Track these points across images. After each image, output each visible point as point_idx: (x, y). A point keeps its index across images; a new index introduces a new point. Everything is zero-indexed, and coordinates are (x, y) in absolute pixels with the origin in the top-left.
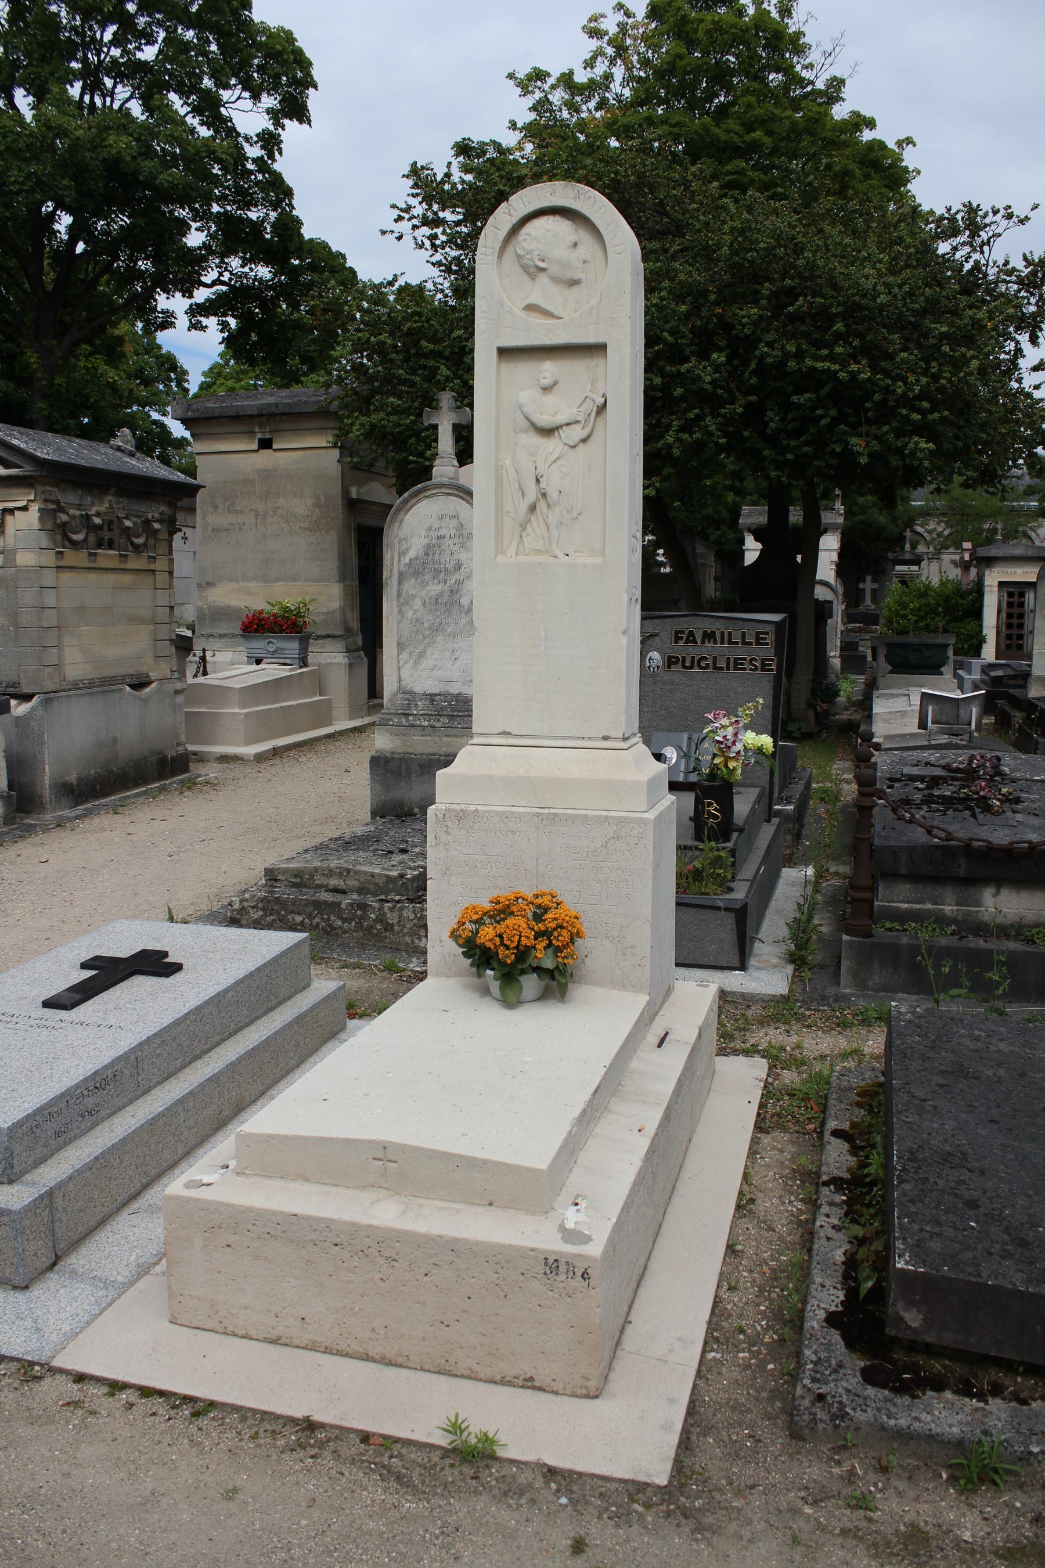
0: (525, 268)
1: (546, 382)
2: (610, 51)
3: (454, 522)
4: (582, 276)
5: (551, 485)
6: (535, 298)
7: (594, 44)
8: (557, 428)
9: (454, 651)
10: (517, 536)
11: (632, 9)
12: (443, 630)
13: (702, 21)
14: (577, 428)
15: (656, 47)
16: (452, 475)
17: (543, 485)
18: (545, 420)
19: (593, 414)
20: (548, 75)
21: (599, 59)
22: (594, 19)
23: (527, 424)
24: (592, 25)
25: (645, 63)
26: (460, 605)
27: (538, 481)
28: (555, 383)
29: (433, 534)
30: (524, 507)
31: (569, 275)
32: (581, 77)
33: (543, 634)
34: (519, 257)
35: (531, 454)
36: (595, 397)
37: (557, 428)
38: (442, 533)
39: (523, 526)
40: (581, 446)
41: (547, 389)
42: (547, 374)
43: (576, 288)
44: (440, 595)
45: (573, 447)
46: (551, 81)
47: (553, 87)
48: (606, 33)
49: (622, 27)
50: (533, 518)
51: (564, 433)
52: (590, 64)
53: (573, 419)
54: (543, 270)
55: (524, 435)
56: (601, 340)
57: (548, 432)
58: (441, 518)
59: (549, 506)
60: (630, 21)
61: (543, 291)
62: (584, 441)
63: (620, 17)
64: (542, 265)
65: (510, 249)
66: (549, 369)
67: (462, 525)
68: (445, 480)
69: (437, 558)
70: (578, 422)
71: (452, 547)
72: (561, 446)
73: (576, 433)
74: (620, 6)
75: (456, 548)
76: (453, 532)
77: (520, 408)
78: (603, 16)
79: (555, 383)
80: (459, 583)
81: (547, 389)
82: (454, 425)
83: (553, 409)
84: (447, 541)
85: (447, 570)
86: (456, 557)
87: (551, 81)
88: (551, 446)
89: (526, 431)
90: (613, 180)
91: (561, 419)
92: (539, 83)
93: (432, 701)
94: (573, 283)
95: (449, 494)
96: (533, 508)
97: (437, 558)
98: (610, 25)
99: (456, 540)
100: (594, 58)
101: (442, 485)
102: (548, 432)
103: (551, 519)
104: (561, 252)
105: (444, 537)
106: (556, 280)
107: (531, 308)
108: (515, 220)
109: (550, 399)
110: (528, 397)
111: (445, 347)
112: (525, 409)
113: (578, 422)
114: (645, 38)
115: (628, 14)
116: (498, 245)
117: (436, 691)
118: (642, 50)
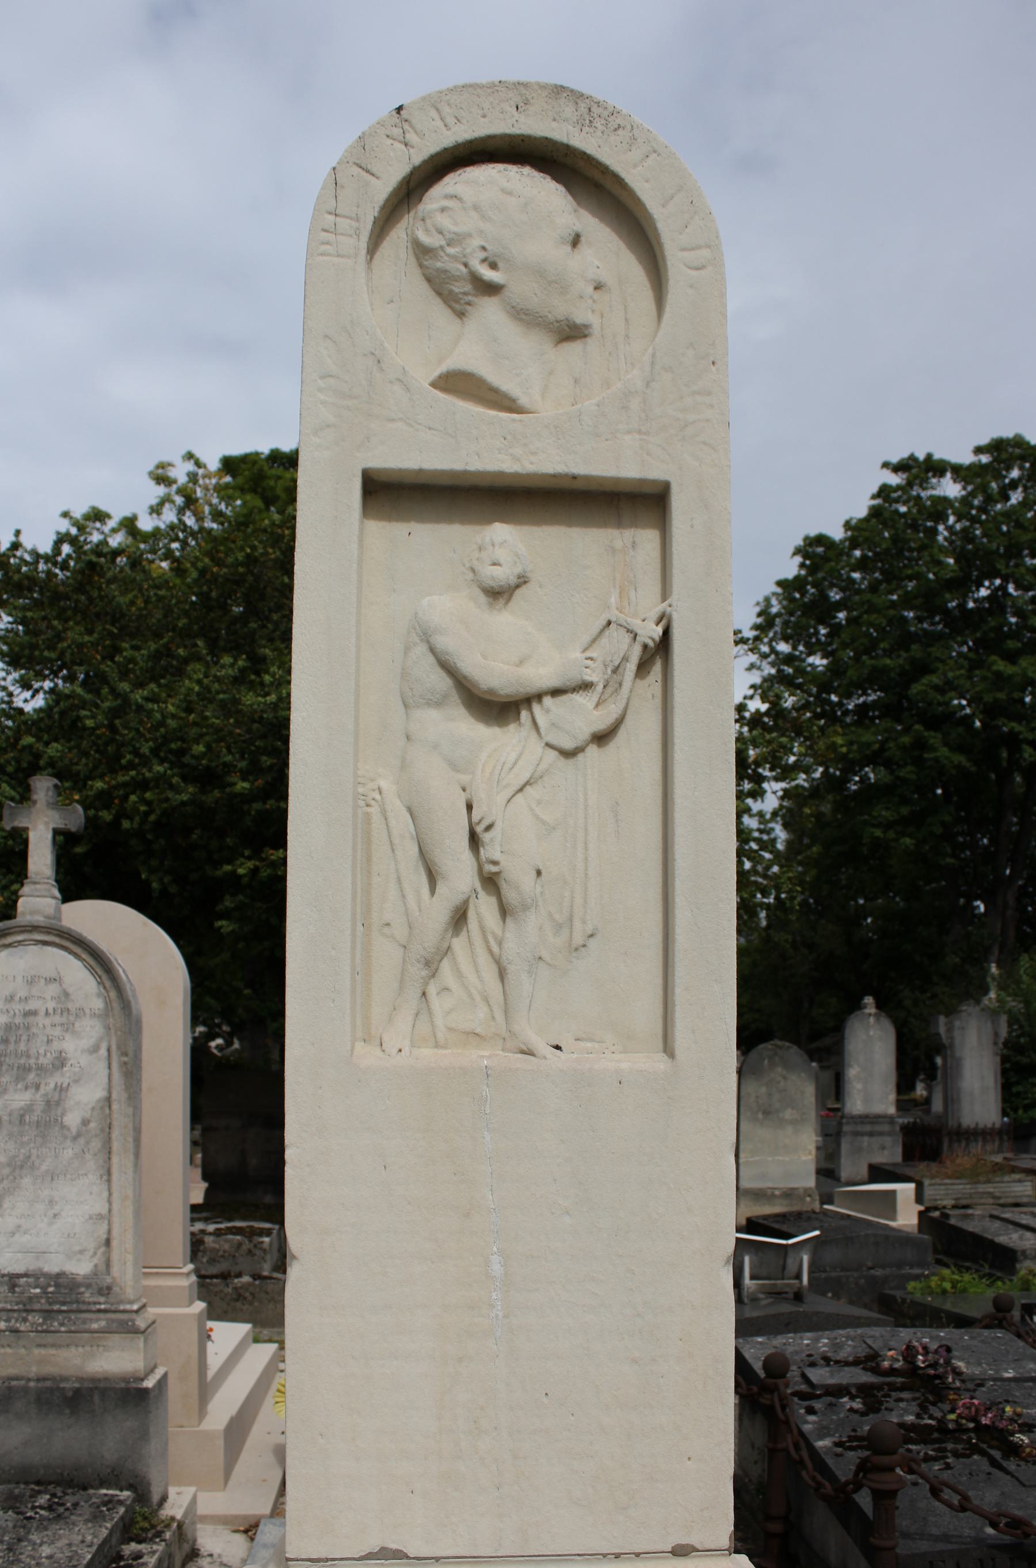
0: (439, 284)
1: (502, 575)
2: (179, 500)
3: (53, 989)
4: (593, 320)
5: (514, 848)
6: (469, 354)
7: (161, 490)
8: (539, 697)
9: (51, 1202)
10: (413, 994)
11: (203, 458)
12: (33, 1167)
13: (279, 478)
14: (583, 700)
15: (229, 500)
16: (51, 911)
17: (491, 850)
18: (496, 674)
19: (632, 667)
20: (109, 516)
21: (167, 505)
22: (162, 466)
23: (443, 683)
24: (160, 471)
25: (217, 515)
26: (63, 1127)
27: (474, 840)
28: (522, 581)
29: (17, 1007)
30: (437, 912)
31: (560, 309)
32: (146, 524)
33: (497, 1269)
34: (422, 251)
35: (454, 767)
36: (636, 624)
37: (539, 697)
38: (32, 1005)
39: (431, 965)
40: (593, 750)
41: (498, 594)
42: (501, 554)
43: (574, 348)
44: (29, 1109)
45: (569, 754)
46: (111, 524)
47: (114, 531)
48: (175, 482)
49: (193, 478)
50: (458, 944)
51: (546, 712)
52: (156, 510)
53: (575, 675)
54: (491, 289)
55: (433, 714)
56: (655, 472)
57: (499, 708)
58: (31, 982)
59: (504, 911)
60: (201, 472)
61: (486, 342)
62: (601, 738)
63: (190, 466)
64: (488, 274)
65: (398, 235)
66: (506, 543)
67: (67, 995)
68: (39, 919)
69: (22, 1047)
70: (586, 686)
71: (49, 1030)
72: (535, 747)
73: (581, 715)
74: (190, 456)
75: (57, 1032)
76: (51, 1005)
77: (426, 638)
78: (170, 465)
79: (522, 581)
80: (62, 1089)
81: (498, 594)
82: (56, 832)
83: (507, 650)
84: (41, 1020)
85: (40, 1068)
86: (56, 1045)
87: (111, 524)
88: (510, 746)
89: (439, 703)
90: (248, 556)
91: (541, 674)
92: (98, 525)
93: (13, 1287)
94: (571, 333)
95: (45, 943)
96: (459, 918)
97: (22, 1047)
98: (180, 473)
99: (57, 1019)
100: (162, 503)
101: (34, 928)
102: (499, 708)
103: (512, 949)
104: (544, 248)
105: (34, 1013)
106: (526, 317)
107: (458, 383)
108: (418, 157)
109: (505, 621)
110: (452, 613)
111: (8, 762)
112: (444, 642)
113: (586, 686)
114: (219, 489)
115: (198, 464)
116: (371, 212)
117: (19, 1268)
118: (215, 501)
